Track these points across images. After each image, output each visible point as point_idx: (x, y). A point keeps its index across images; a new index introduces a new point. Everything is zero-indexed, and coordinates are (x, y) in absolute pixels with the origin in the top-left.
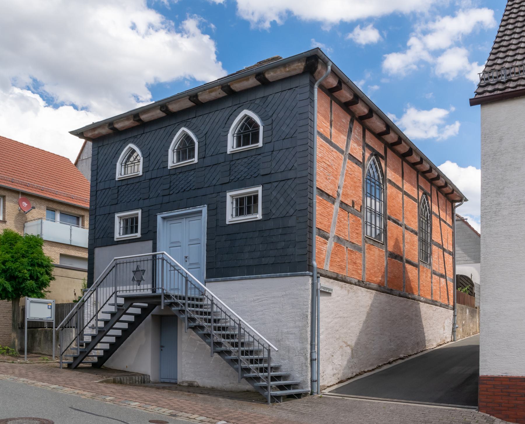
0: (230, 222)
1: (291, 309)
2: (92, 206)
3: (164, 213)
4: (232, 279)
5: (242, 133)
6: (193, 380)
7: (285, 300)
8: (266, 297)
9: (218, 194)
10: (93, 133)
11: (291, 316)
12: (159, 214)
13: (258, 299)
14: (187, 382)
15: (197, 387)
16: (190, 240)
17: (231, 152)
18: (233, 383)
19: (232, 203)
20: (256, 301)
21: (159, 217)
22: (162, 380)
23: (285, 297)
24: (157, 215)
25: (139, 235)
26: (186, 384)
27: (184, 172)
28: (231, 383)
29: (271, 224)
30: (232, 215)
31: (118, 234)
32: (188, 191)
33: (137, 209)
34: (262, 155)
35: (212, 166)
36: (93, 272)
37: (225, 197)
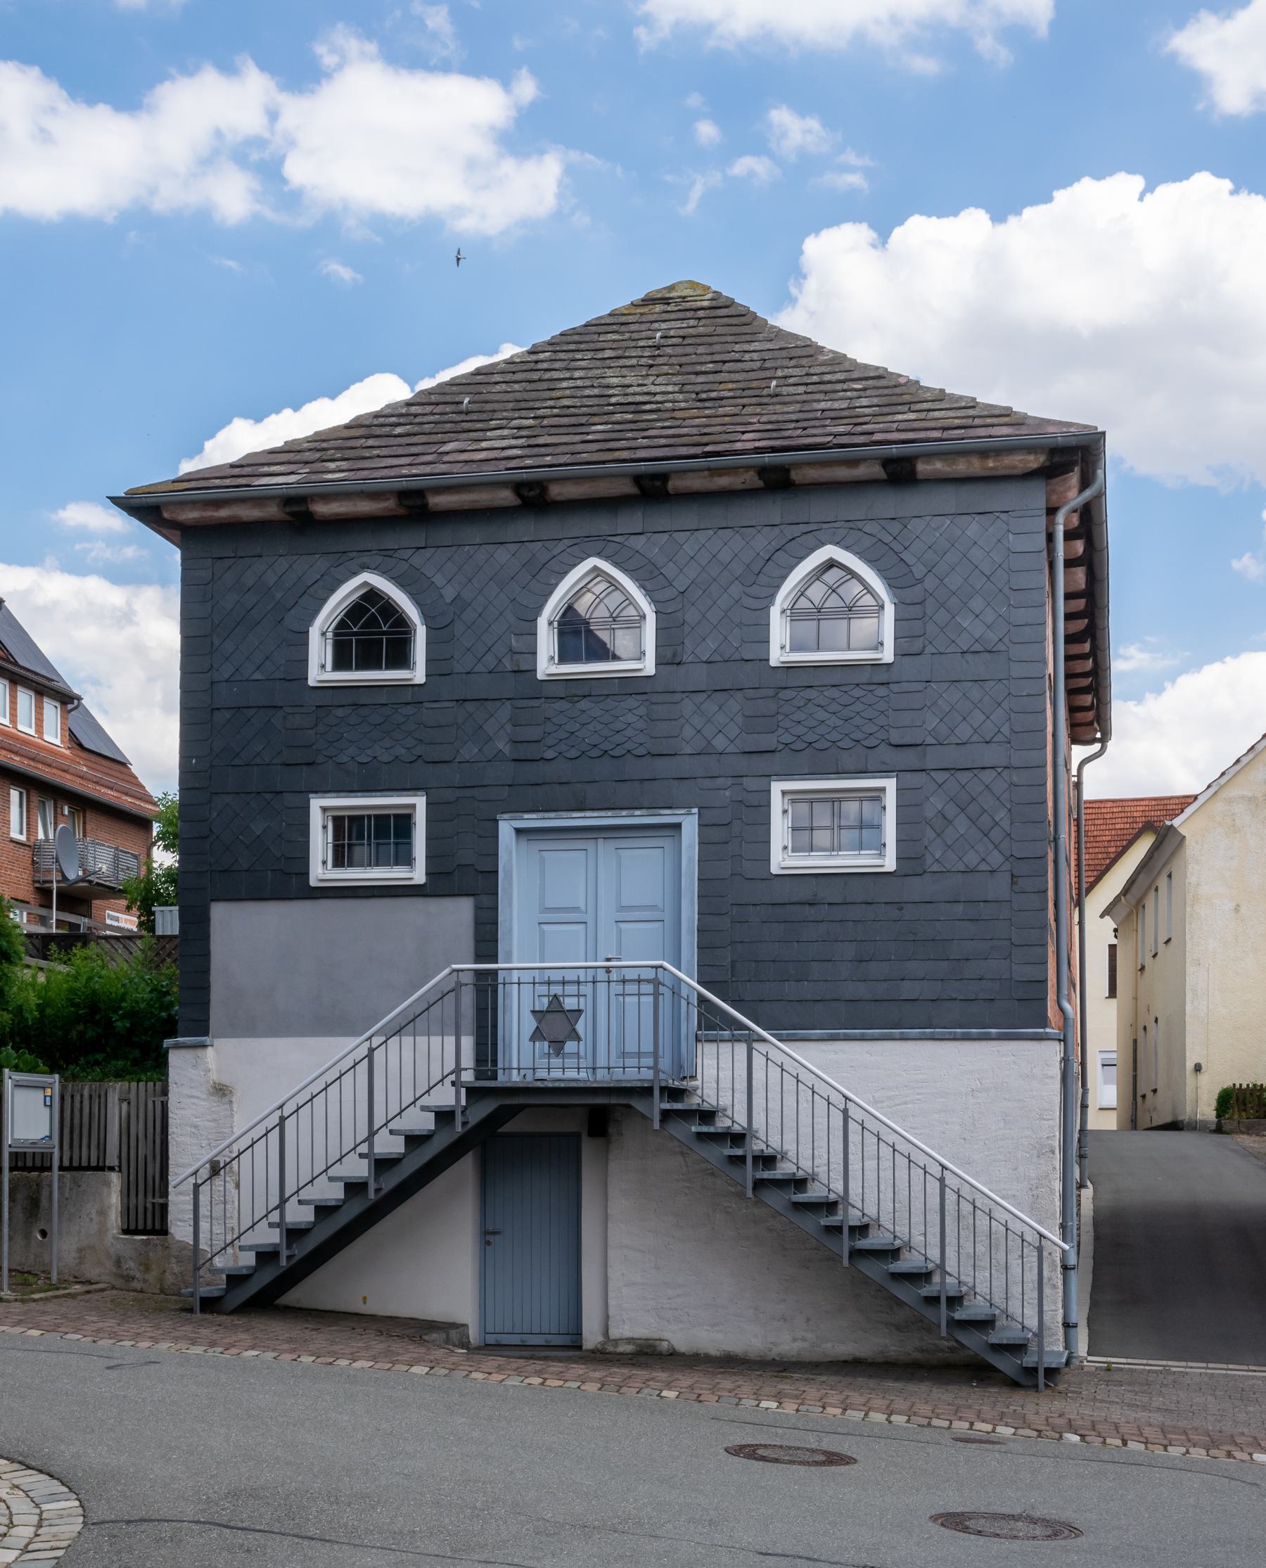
0: (782, 868)
1: (1000, 1129)
2: (193, 757)
3: (526, 816)
4: (798, 1038)
5: (355, 634)
6: (656, 1336)
7: (979, 1104)
8: (918, 1094)
9: (738, 780)
10: (926, 467)
11: (1002, 1149)
12: (505, 816)
13: (889, 1098)
14: (630, 1340)
15: (671, 1354)
16: (622, 908)
17: (782, 662)
18: (804, 1339)
19: (325, 827)
20: (882, 1102)
21: (506, 829)
22: (491, 1339)
23: (979, 1095)
24: (498, 821)
25: (418, 874)
26: (629, 1348)
27: (604, 698)
28: (795, 1340)
29: (915, 889)
30: (324, 863)
31: (321, 870)
32: (613, 757)
33: (413, 789)
34: (894, 687)
35: (709, 693)
36: (208, 982)
37: (306, 810)
